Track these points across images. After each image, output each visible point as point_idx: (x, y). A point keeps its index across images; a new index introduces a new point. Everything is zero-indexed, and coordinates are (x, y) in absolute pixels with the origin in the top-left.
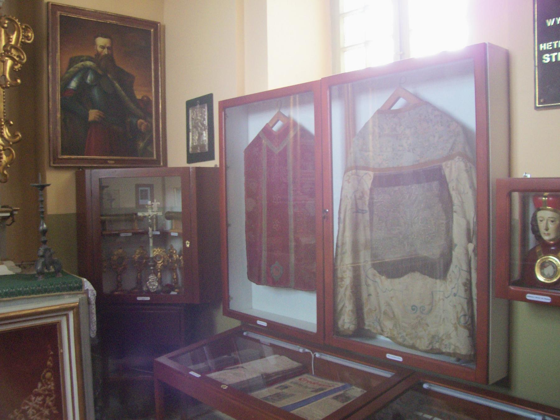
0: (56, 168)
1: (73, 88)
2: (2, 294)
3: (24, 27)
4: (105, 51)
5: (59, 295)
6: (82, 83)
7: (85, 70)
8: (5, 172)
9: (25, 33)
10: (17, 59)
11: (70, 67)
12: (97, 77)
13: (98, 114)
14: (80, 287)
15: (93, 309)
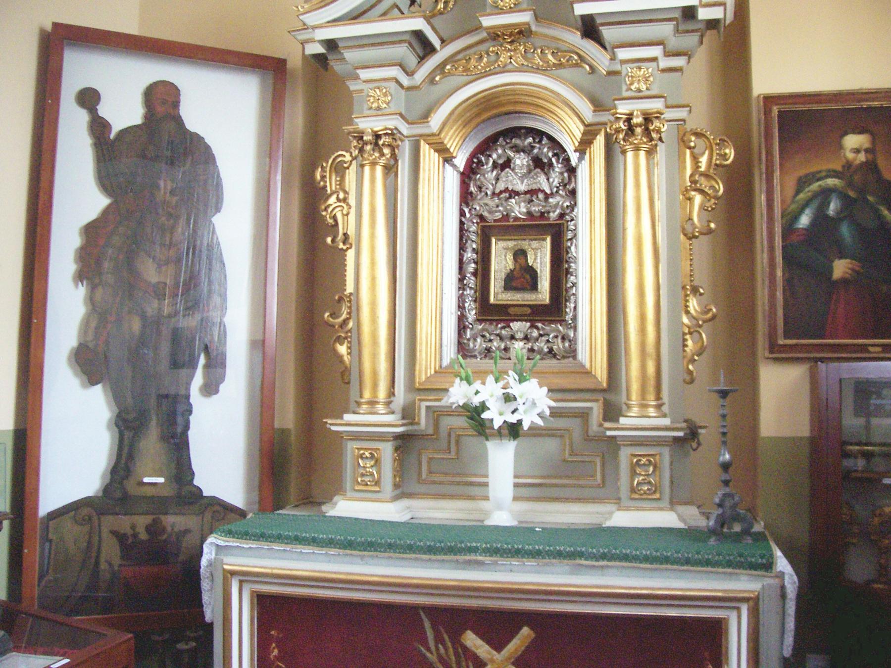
0: (777, 360)
1: (805, 227)
2: (723, 562)
3: (718, 141)
4: (862, 157)
5: (730, 574)
6: (820, 218)
7: (826, 193)
8: (691, 367)
9: (720, 149)
10: (710, 192)
11: (798, 192)
12: (847, 202)
13: (850, 266)
14: (768, 566)
15: (790, 607)
